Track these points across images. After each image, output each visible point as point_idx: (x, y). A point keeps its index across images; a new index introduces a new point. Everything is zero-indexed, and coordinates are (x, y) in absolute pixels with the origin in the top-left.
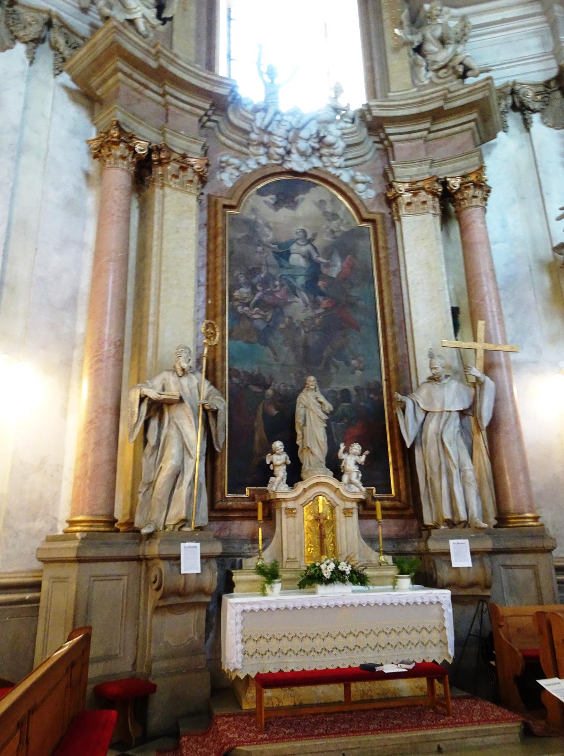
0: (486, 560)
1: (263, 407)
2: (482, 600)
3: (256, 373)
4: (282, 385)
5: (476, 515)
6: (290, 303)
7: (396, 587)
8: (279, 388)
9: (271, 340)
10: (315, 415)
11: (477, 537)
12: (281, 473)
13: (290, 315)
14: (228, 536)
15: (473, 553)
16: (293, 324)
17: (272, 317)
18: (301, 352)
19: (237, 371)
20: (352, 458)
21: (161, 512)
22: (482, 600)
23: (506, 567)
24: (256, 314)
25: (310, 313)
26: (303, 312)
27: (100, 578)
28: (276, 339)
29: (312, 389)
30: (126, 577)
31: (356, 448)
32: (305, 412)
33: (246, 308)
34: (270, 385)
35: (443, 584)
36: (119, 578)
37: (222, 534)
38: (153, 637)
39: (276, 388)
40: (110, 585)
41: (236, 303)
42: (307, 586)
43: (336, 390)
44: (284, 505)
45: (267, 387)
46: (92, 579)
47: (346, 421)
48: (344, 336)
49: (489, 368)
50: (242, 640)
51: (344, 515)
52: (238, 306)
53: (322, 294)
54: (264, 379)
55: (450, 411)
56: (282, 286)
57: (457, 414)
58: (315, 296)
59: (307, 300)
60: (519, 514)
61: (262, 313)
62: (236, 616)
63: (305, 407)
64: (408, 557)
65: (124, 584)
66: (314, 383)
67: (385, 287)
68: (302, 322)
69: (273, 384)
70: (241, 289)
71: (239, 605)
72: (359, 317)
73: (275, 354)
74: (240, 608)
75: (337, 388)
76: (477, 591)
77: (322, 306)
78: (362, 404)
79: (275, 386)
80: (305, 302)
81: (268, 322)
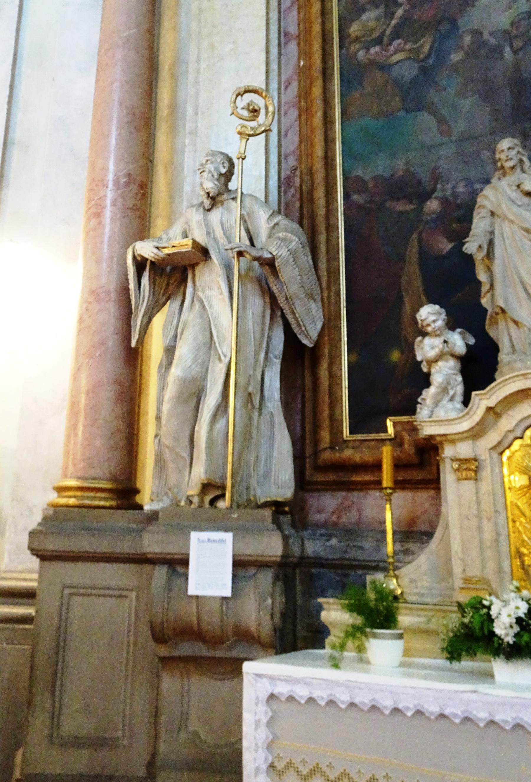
1: (420, 239)
3: (401, 173)
4: (461, 185)
9: (433, 95)
10: (515, 228)
12: (445, 374)
13: (475, 26)
14: (356, 523)
16: (484, 43)
17: (431, 47)
18: (506, 99)
19: (359, 179)
21: (180, 471)
24: (397, 54)
27: (82, 591)
28: (444, 89)
29: (513, 168)
30: (133, 595)
32: (492, 225)
33: (375, 50)
34: (434, 190)
36: (121, 595)
37: (343, 519)
38: (163, 718)
39: (448, 192)
40: (103, 607)
41: (354, 47)
42: (502, 656)
44: (448, 452)
45: (425, 196)
46: (67, 591)
50: (272, 766)
52: (358, 51)
54: (420, 181)
61: (409, 46)
62: (257, 704)
63: (493, 214)
65: (130, 608)
66: (513, 153)
68: (506, 32)
69: (439, 186)
70: (364, 17)
71: (265, 680)
74: (264, 688)
79: (443, 190)
81: (422, 61)
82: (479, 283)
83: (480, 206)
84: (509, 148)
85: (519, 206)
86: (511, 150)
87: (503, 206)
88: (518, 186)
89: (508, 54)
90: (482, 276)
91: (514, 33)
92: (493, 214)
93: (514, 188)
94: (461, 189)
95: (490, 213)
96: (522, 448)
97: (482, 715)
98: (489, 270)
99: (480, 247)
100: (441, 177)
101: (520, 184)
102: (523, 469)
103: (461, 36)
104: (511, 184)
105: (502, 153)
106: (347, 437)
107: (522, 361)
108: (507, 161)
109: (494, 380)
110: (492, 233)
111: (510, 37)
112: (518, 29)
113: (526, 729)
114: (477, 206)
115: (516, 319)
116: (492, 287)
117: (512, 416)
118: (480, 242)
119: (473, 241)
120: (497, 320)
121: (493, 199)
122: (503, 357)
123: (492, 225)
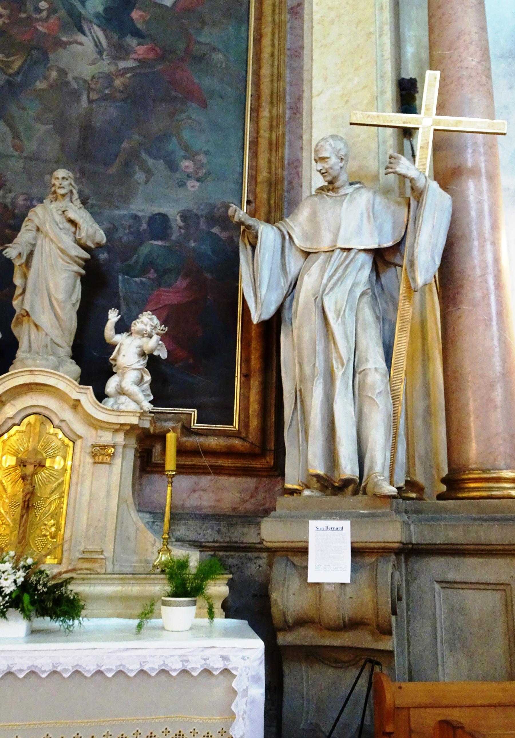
0: (387, 568)
2: (371, 661)
4: (22, 197)
5: (378, 468)
6: (65, 45)
7: (153, 622)
8: (13, 203)
9: (14, 109)
10: (53, 246)
11: (373, 515)
13: (62, 66)
15: (357, 552)
16: (67, 84)
18: (75, 138)
20: (136, 343)
22: (371, 661)
23: (447, 584)
25: (105, 66)
26: (93, 63)
28: (23, 109)
29: (63, 195)
31: (146, 321)
35: (286, 621)
39: (9, 200)
43: (140, 214)
47: (152, 274)
48: (172, 115)
49: (449, 175)
51: (91, 460)
53: (137, 33)
55: (349, 250)
56: (52, 10)
57: (367, 260)
58: (122, 36)
59: (104, 42)
60: (484, 471)
63: (38, 229)
64: (250, 554)
66: (66, 183)
67: (267, 30)
68: (86, 81)
72: (206, 82)
73: (16, 136)
75: (143, 210)
76: (363, 640)
77: (133, 56)
78: (193, 244)
80: (97, 44)
81: (10, 75)
82: (15, 286)
83: (29, 220)
84: (63, 178)
85: (61, 229)
86: (65, 180)
87: (48, 225)
88: (64, 212)
89: (84, 102)
90: (18, 281)
91: (92, 86)
92: (38, 229)
93: (60, 212)
94: (20, 201)
95: (36, 228)
96: (17, 434)
97: (132, 669)
98: (25, 277)
99: (20, 254)
100: (5, 185)
101: (65, 211)
102: (14, 451)
103: (49, 69)
104: (59, 208)
105: (57, 181)
106: (193, 426)
107: (34, 360)
108: (59, 188)
109: (8, 372)
110: (34, 245)
111: (89, 87)
112: (97, 83)
113: (83, 675)
114: (27, 219)
115: (37, 323)
116: (24, 292)
117: (15, 406)
118: (21, 250)
119: (14, 248)
120: (22, 321)
121: (41, 217)
122: (20, 354)
123: (35, 239)
